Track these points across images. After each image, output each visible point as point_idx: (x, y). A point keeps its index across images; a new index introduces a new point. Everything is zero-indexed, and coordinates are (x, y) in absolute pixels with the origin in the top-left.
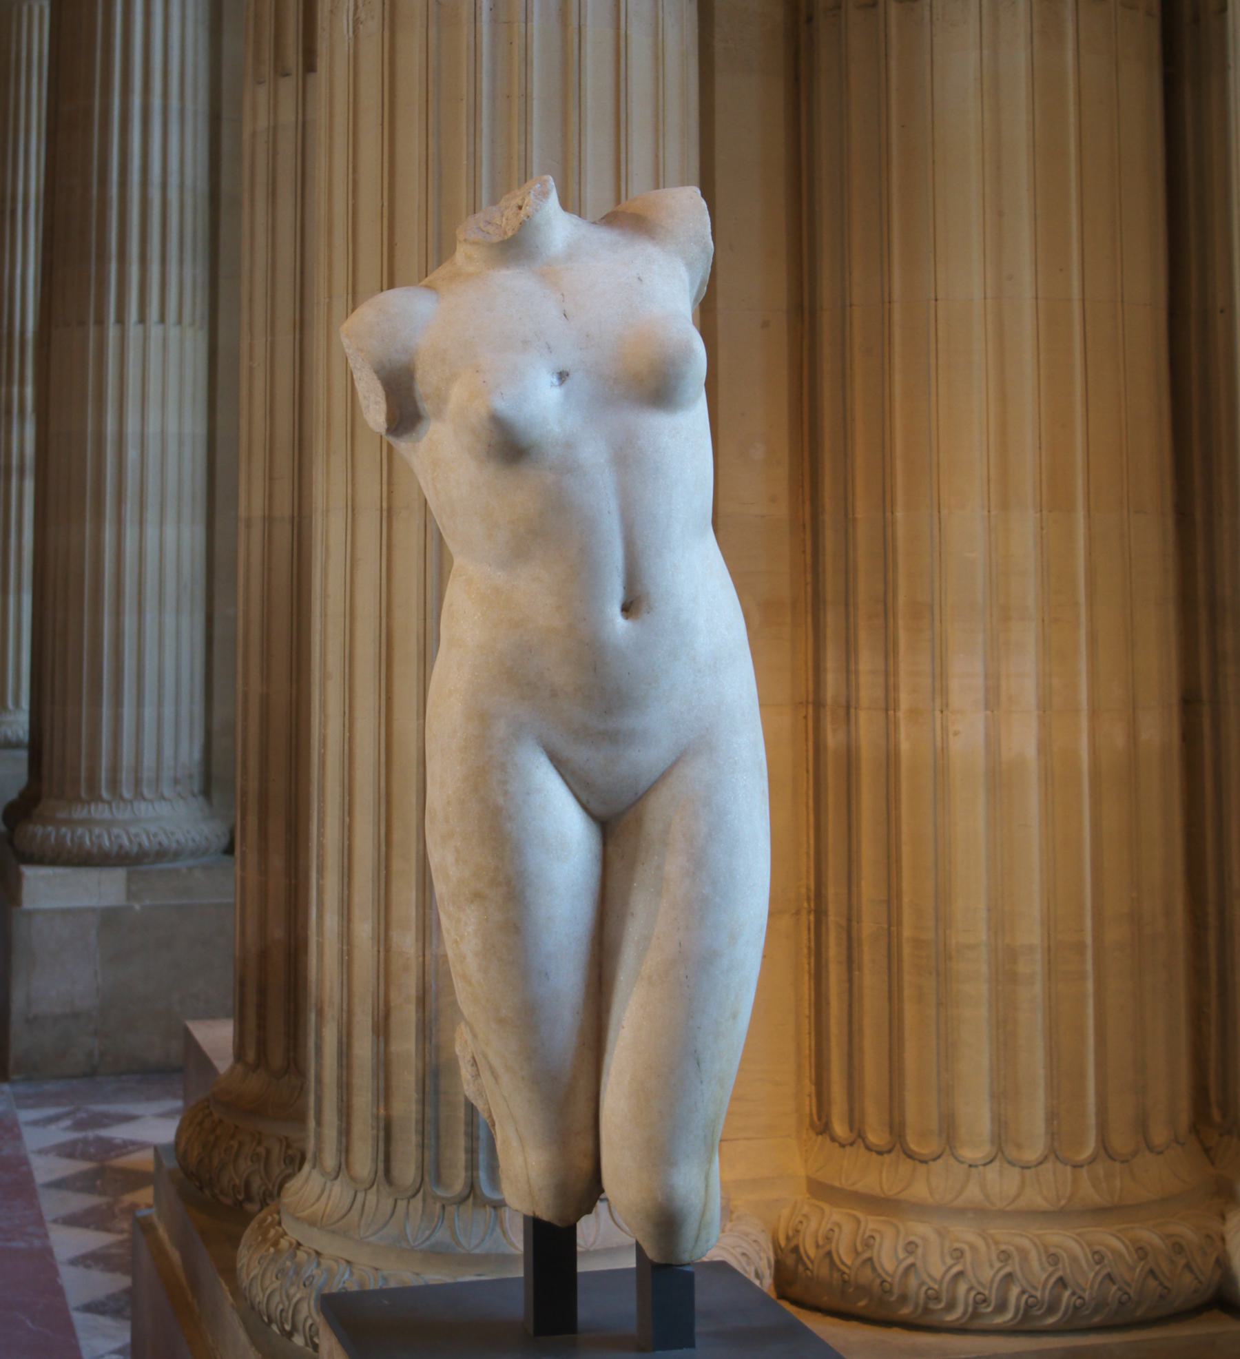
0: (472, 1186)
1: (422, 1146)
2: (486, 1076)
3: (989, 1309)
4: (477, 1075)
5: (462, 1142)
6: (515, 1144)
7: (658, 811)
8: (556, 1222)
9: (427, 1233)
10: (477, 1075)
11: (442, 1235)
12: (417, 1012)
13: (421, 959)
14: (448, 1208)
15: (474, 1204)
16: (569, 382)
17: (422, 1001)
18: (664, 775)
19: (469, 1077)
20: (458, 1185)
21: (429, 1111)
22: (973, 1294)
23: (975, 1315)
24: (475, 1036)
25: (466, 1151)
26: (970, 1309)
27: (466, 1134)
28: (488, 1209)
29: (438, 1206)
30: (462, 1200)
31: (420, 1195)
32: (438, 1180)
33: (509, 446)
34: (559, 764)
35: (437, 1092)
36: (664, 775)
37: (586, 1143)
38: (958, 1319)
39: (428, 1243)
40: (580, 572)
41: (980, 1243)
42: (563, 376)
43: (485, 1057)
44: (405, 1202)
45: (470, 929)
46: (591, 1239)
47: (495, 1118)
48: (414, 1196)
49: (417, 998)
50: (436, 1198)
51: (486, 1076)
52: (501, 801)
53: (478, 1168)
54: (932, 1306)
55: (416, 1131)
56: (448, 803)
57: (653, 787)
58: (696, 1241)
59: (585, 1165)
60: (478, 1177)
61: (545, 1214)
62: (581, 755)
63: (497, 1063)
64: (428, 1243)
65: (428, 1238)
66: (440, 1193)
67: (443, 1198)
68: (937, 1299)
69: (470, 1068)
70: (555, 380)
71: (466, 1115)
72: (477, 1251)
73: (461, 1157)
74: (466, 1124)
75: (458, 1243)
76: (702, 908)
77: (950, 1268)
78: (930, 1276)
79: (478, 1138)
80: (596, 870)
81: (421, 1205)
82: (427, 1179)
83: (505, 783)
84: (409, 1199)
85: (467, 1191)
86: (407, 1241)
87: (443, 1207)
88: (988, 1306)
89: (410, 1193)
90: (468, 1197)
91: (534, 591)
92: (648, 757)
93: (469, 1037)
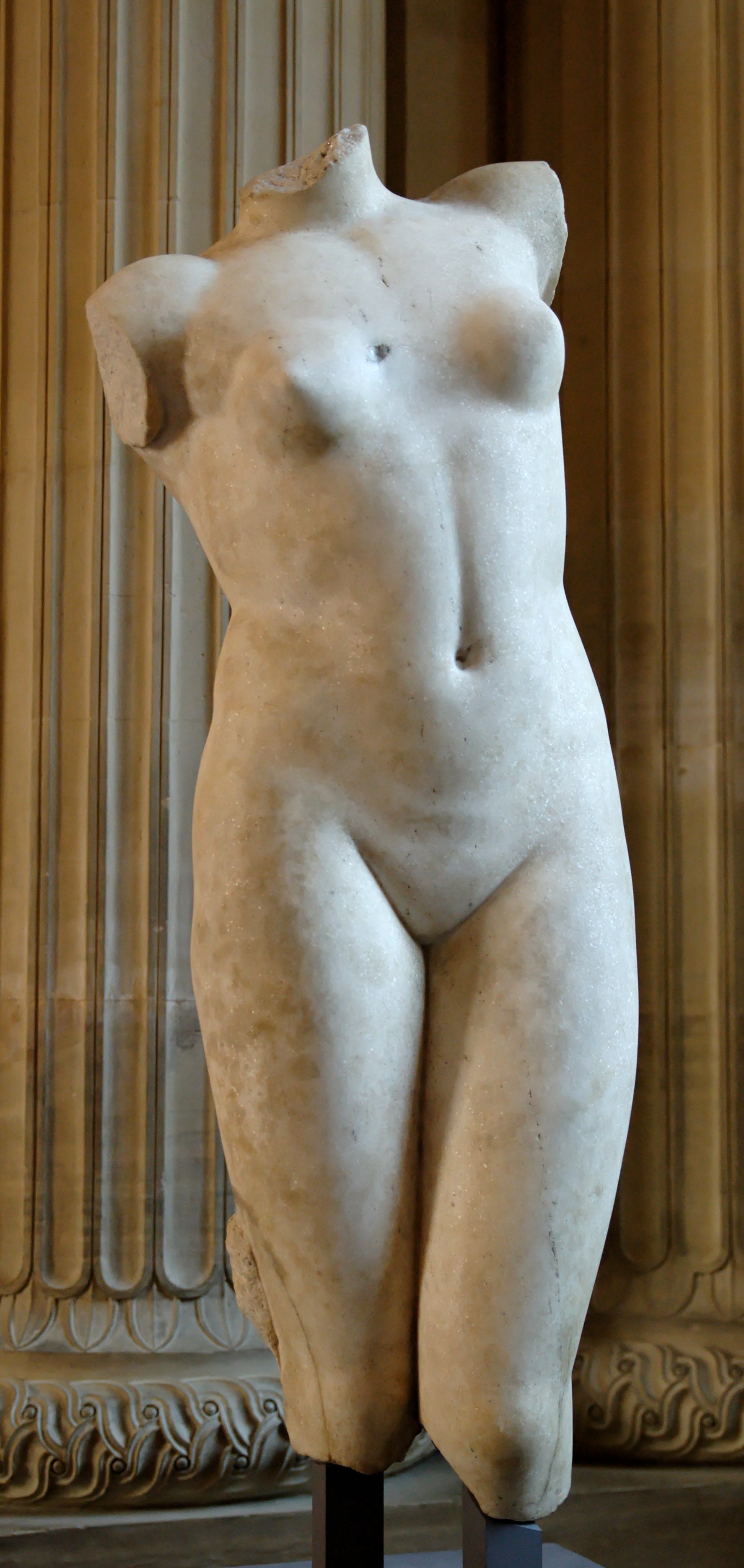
0: (92, 1275)
1: (32, 1230)
2: (268, 1276)
3: (719, 1434)
4: (256, 1277)
5: (80, 1222)
6: (306, 1364)
7: (502, 933)
8: (358, 1468)
9: (36, 1332)
10: (256, 1277)
11: (53, 1334)
12: (28, 1068)
13: (33, 1005)
14: (62, 1304)
15: (93, 1297)
16: (389, 358)
17: (34, 1054)
18: (509, 882)
19: (244, 1280)
20: (75, 1275)
21: (41, 1190)
22: (700, 1414)
23: (703, 1442)
24: (254, 1221)
25: (86, 1233)
26: (696, 1435)
27: (85, 1212)
28: (111, 1302)
29: (50, 1301)
30: (78, 1294)
31: (28, 1291)
32: (51, 1268)
33: (311, 433)
34: (370, 856)
35: (50, 1164)
36: (509, 882)
37: (397, 1363)
38: (682, 1449)
39: (36, 1343)
40: (396, 607)
41: (710, 1359)
42: (382, 352)
43: (268, 1248)
44: (10, 1298)
45: (252, 1074)
46: (238, 1338)
47: (278, 1334)
48: (21, 1290)
49: (28, 1051)
50: (47, 1291)
51: (268, 1276)
52: (295, 901)
53: (98, 1253)
54: (651, 1432)
55: (25, 1213)
56: (225, 907)
57: (491, 899)
58: (545, 1490)
59: (399, 1391)
60: (99, 1263)
61: (344, 1459)
62: (402, 848)
63: (283, 1254)
64: (36, 1343)
65: (35, 1339)
66: (53, 1284)
67: (55, 1291)
68: (657, 1421)
69: (245, 1269)
70: (372, 353)
71: (85, 1190)
72: (96, 1350)
73: (79, 1241)
74: (86, 1201)
75: (74, 1343)
76: (545, 1051)
77: (672, 1386)
78: (649, 1396)
79: (99, 1217)
80: (418, 1004)
81: (28, 1302)
82: (36, 1268)
83: (301, 877)
84: (15, 1295)
85: (85, 1282)
86: (11, 1342)
87: (57, 1301)
88: (718, 1429)
89: (16, 1287)
90: (86, 1289)
91: (338, 624)
92: (488, 854)
93: (246, 1227)
